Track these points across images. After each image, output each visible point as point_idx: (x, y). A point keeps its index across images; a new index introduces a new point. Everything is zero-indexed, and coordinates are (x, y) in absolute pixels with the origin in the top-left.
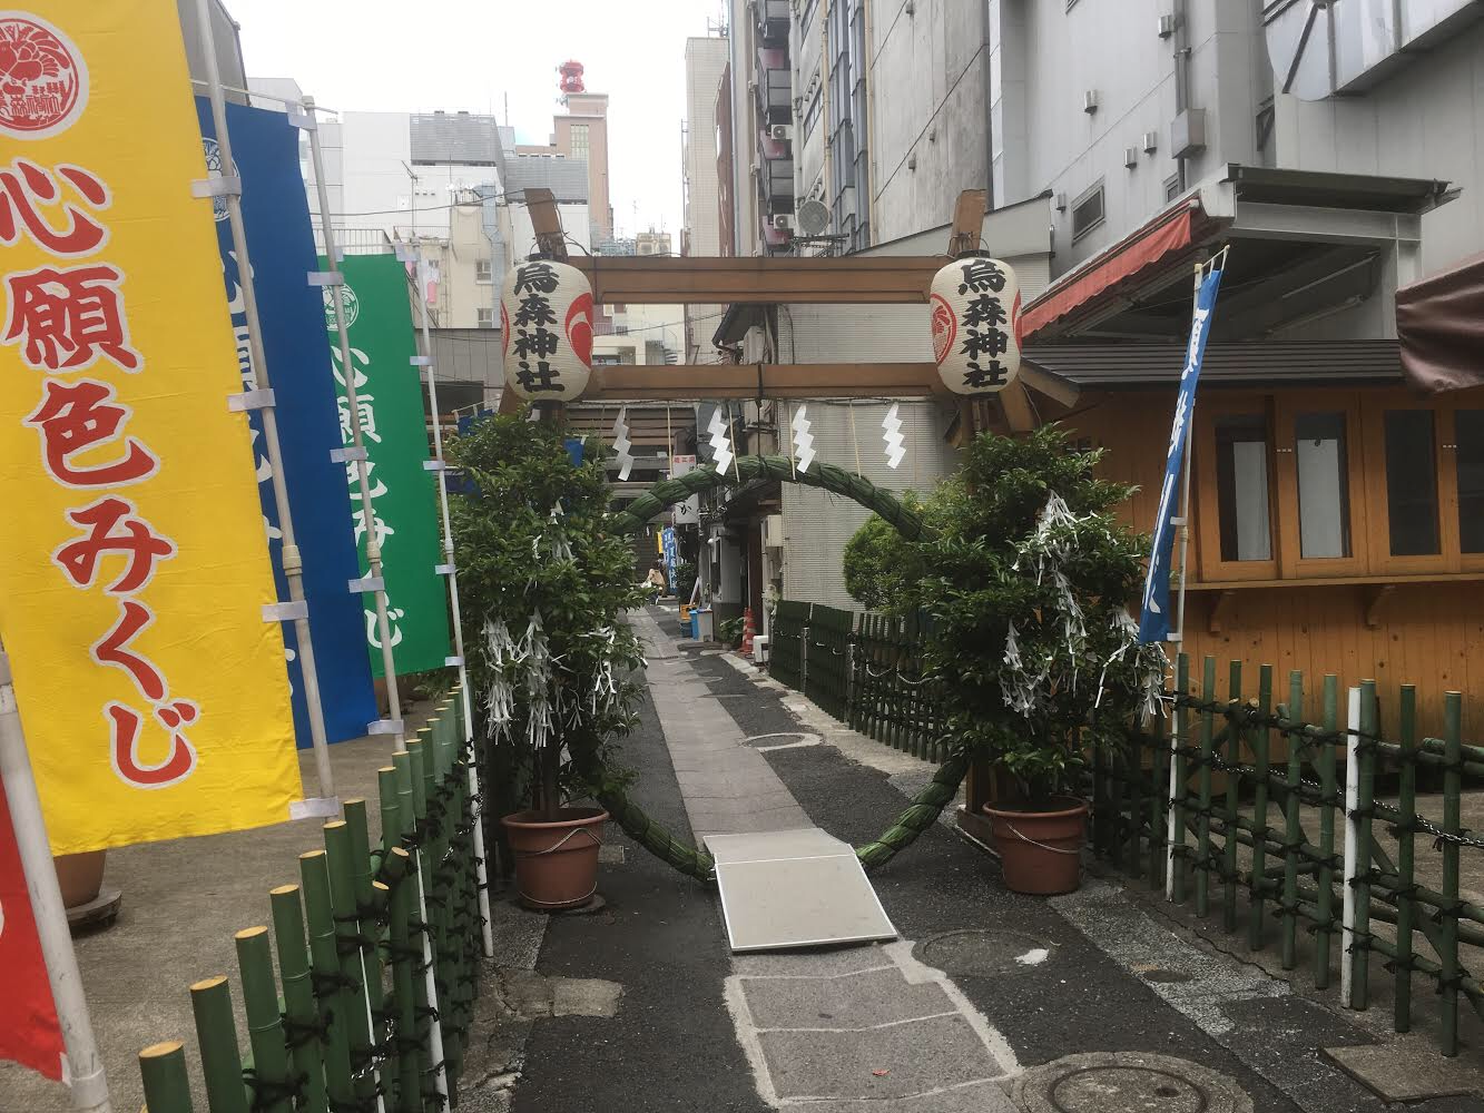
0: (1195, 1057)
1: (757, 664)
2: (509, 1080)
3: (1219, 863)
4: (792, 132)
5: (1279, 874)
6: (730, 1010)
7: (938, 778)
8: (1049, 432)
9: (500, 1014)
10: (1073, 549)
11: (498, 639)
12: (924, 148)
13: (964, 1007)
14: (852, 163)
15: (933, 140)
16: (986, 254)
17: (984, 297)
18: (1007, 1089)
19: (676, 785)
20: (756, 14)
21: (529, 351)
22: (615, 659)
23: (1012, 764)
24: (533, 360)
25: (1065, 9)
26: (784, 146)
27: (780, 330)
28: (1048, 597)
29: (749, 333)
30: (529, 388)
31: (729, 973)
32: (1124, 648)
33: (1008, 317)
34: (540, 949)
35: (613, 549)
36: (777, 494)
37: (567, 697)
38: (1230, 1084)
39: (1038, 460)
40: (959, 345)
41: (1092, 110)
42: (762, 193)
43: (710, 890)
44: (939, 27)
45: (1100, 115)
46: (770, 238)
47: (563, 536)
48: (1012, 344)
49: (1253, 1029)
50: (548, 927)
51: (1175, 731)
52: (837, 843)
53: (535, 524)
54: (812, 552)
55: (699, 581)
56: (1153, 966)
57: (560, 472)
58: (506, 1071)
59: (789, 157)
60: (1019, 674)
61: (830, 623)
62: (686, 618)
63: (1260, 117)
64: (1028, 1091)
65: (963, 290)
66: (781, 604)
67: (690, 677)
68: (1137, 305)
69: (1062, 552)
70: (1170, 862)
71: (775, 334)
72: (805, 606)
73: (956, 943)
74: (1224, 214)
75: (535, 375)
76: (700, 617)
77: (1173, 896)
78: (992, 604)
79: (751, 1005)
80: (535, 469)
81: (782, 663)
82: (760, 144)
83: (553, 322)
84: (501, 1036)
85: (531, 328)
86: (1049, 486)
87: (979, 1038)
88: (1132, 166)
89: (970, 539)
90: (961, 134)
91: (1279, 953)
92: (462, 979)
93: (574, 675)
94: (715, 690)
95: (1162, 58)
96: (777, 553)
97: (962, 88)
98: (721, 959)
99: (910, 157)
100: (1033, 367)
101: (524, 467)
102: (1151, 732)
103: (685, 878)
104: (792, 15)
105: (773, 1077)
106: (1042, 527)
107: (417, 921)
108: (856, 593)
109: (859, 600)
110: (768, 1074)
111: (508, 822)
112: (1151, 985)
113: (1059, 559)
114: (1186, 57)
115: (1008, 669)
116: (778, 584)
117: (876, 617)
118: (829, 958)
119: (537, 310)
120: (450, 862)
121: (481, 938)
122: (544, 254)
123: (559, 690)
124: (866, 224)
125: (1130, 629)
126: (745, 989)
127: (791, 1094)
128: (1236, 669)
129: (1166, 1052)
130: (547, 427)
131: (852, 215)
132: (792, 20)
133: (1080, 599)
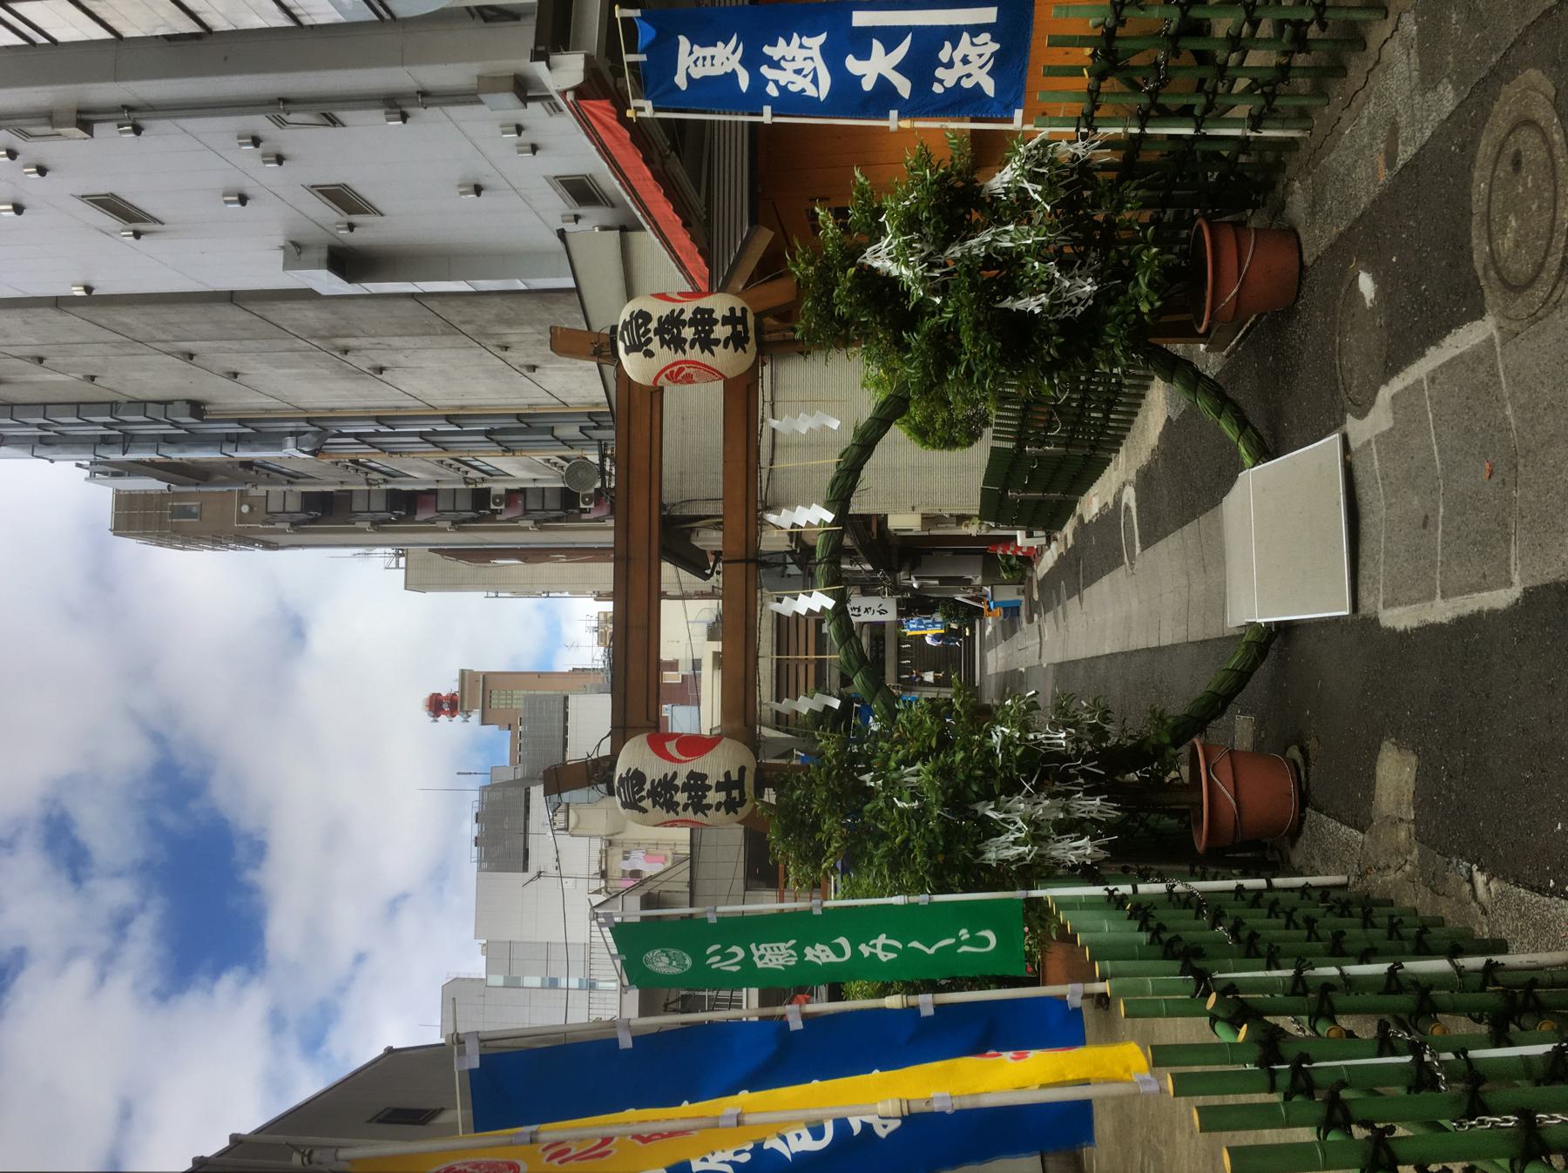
0: (1478, 125)
1: (1049, 543)
2: (1480, 879)
3: (1268, 83)
4: (498, 488)
5: (1280, 25)
6: (1415, 625)
7: (1168, 379)
8: (797, 266)
9: (1410, 879)
10: (920, 240)
11: (999, 851)
12: (516, 357)
13: (1419, 370)
14: (529, 429)
15: (506, 348)
16: (614, 329)
17: (650, 794)
18: (1509, 336)
19: (1174, 646)
20: (384, 522)
22: (1025, 728)
23: (1151, 304)
24: (713, 797)
25: (378, 218)
26: (512, 496)
28: (971, 267)
29: (697, 544)
30: (742, 802)
31: (1376, 620)
32: (1026, 185)
33: (677, 307)
34: (1342, 823)
35: (910, 722)
36: (865, 518)
37: (1065, 777)
38: (1510, 91)
39: (826, 280)
40: (705, 358)
41: (478, 190)
42: (558, 519)
43: (1284, 631)
44: (396, 342)
45: (483, 182)
46: (604, 511)
47: (895, 775)
48: (705, 303)
49: (1450, 58)
50: (1319, 810)
51: (1120, 130)
52: (1237, 488)
53: (882, 804)
54: (930, 483)
55: (959, 598)
56: (1380, 161)
57: (828, 774)
58: (1471, 880)
59: (523, 491)
60: (1052, 298)
61: (1002, 470)
62: (999, 612)
63: (486, 19)
64: (1511, 313)
65: (649, 354)
66: (983, 516)
67: (1061, 615)
68: (674, 148)
69: (922, 251)
70: (1266, 133)
72: (985, 493)
73: (1351, 371)
74: (581, 65)
75: (729, 795)
76: (997, 599)
77: (1305, 130)
78: (977, 326)
79: (1411, 602)
80: (825, 801)
81: (1049, 518)
82: (509, 520)
83: (675, 775)
84: (1434, 882)
85: (681, 797)
86: (852, 265)
87: (1453, 359)
88: (534, 149)
89: (907, 348)
91: (1367, 22)
92: (1367, 921)
93: (1042, 769)
94: (1075, 591)
95: (428, 119)
96: (928, 519)
98: (1359, 627)
99: (524, 371)
100: (727, 280)
101: (823, 811)
102: (1121, 153)
103: (1272, 654)
104: (383, 487)
105: (1489, 589)
106: (895, 273)
107: (1290, 983)
108: (973, 437)
109: (981, 434)
110: (1485, 594)
111: (1201, 845)
112: (1400, 164)
113: (930, 254)
114: (426, 97)
115: (1051, 309)
116: (961, 519)
117: (998, 417)
118: (1364, 509)
119: (663, 792)
120: (1234, 931)
121: (1325, 890)
122: (609, 781)
123: (1058, 786)
124: (590, 415)
125: (1006, 178)
126: (1393, 605)
127: (1508, 572)
128: (1052, 71)
129: (1473, 158)
130: (782, 784)
131: (582, 429)
132: (389, 487)
133: (974, 230)
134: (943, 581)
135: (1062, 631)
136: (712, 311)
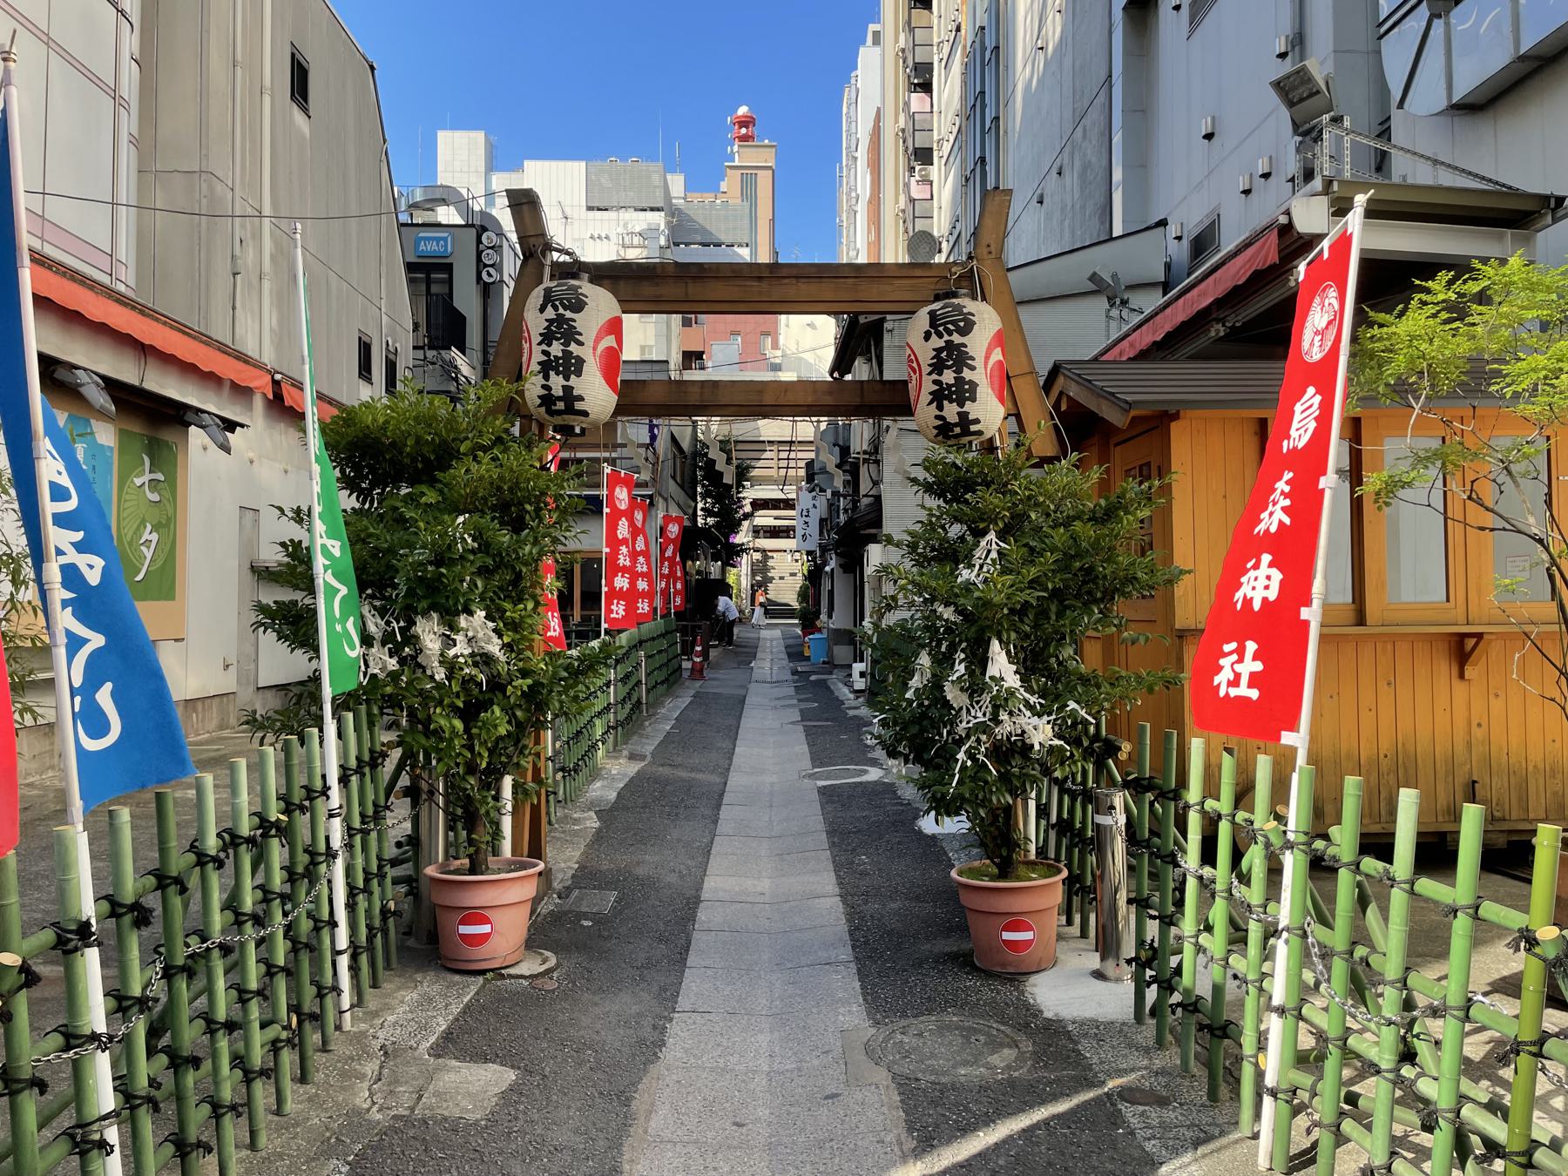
17: (561, 316)
21: (552, 373)
27: (886, 359)
30: (551, 413)
65: (927, 336)
71: (880, 364)
75: (559, 399)
83: (580, 344)
90: (1086, 167)
97: (1087, 121)
104: (936, 59)
134: (1312, 459)
135: (774, 703)
136: (974, 400)
